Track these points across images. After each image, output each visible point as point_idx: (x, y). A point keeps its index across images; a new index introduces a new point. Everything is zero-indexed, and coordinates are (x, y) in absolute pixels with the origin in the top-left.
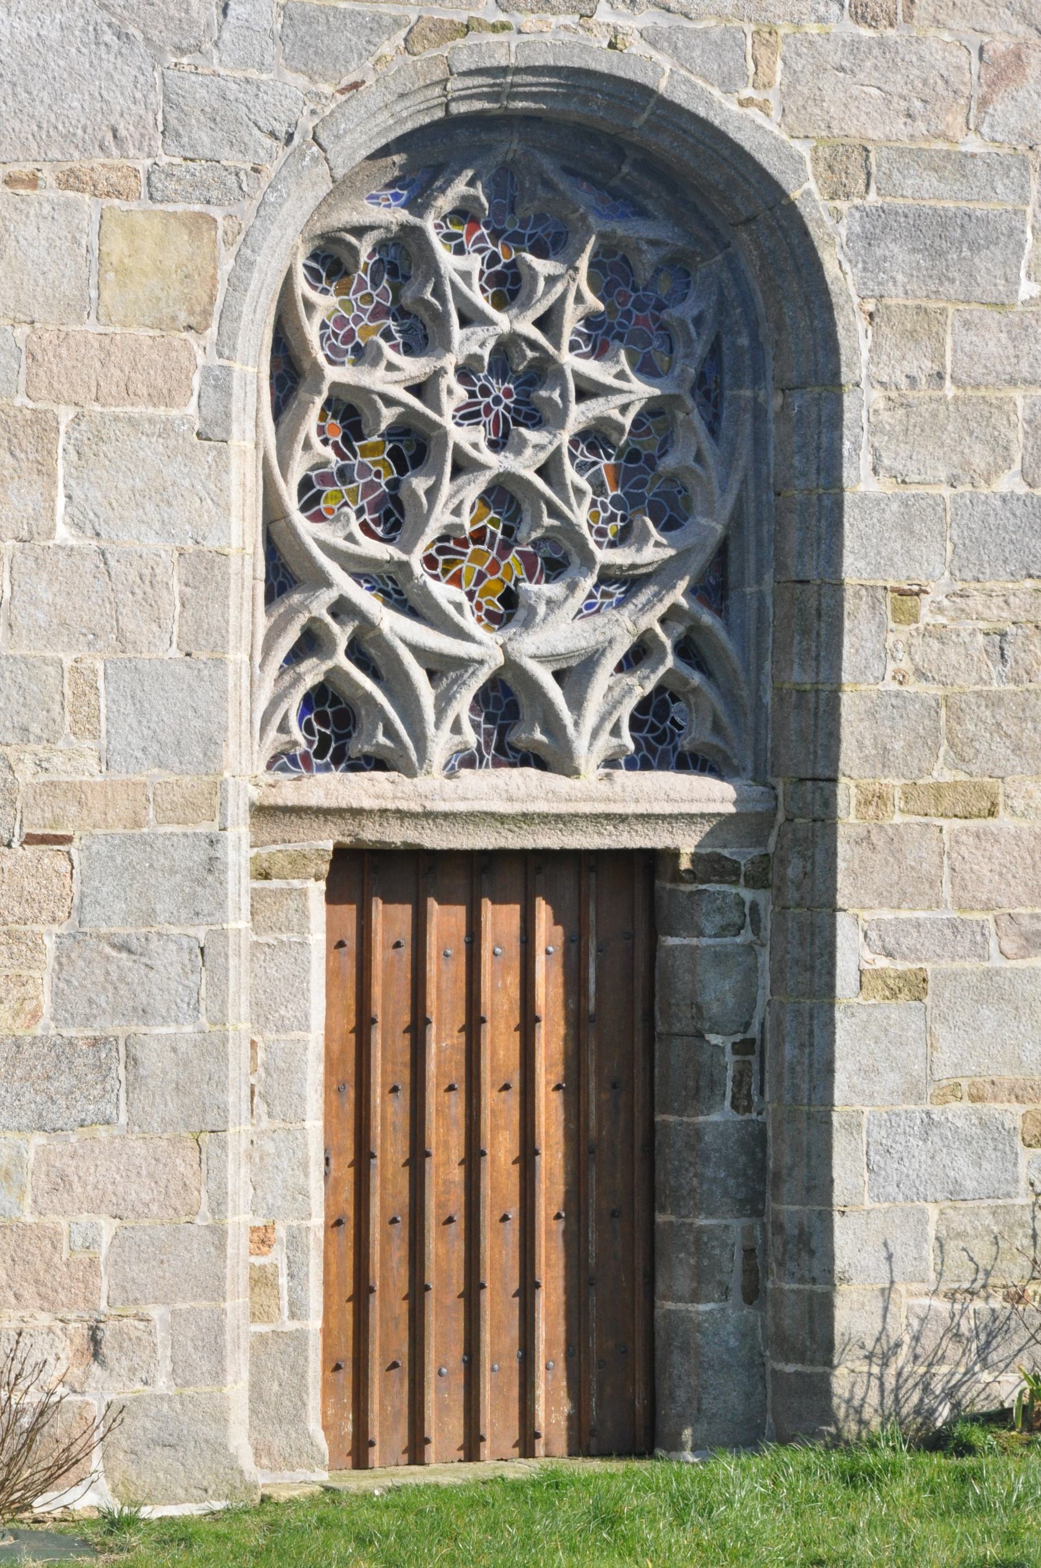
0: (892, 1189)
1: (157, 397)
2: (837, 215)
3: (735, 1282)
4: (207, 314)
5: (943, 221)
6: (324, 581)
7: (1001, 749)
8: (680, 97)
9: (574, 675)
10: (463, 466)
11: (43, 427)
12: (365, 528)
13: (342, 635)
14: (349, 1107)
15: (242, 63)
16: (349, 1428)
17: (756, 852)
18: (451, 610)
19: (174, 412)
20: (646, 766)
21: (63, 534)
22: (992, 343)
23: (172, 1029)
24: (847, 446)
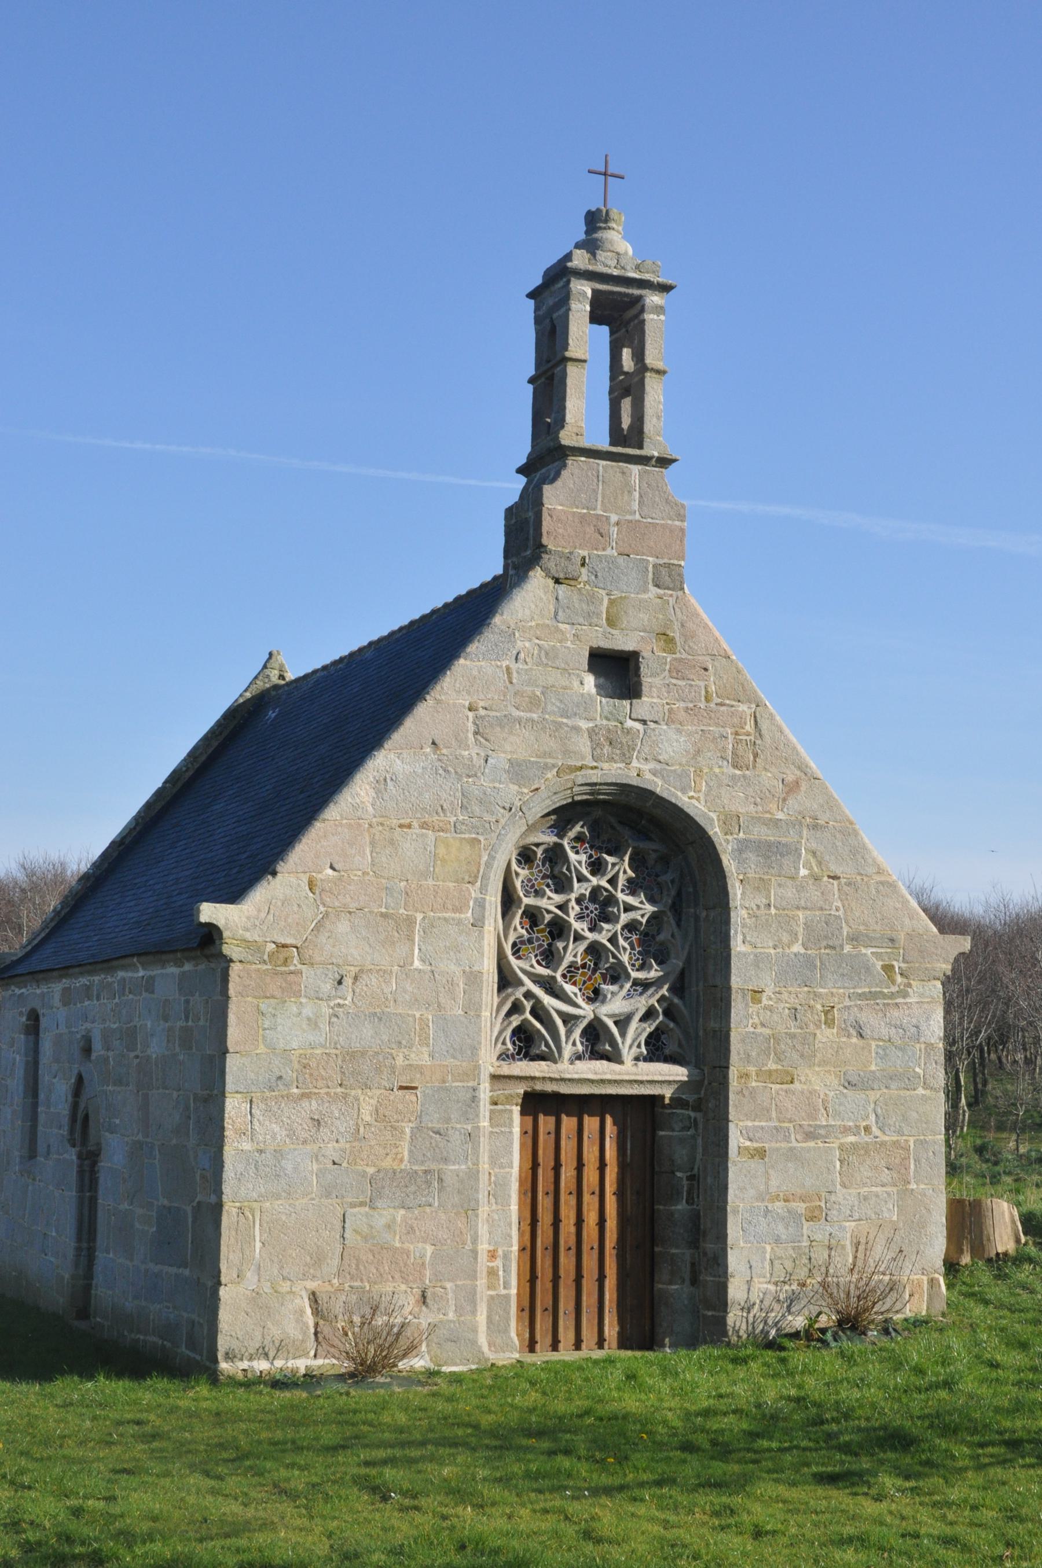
12: (538, 962)
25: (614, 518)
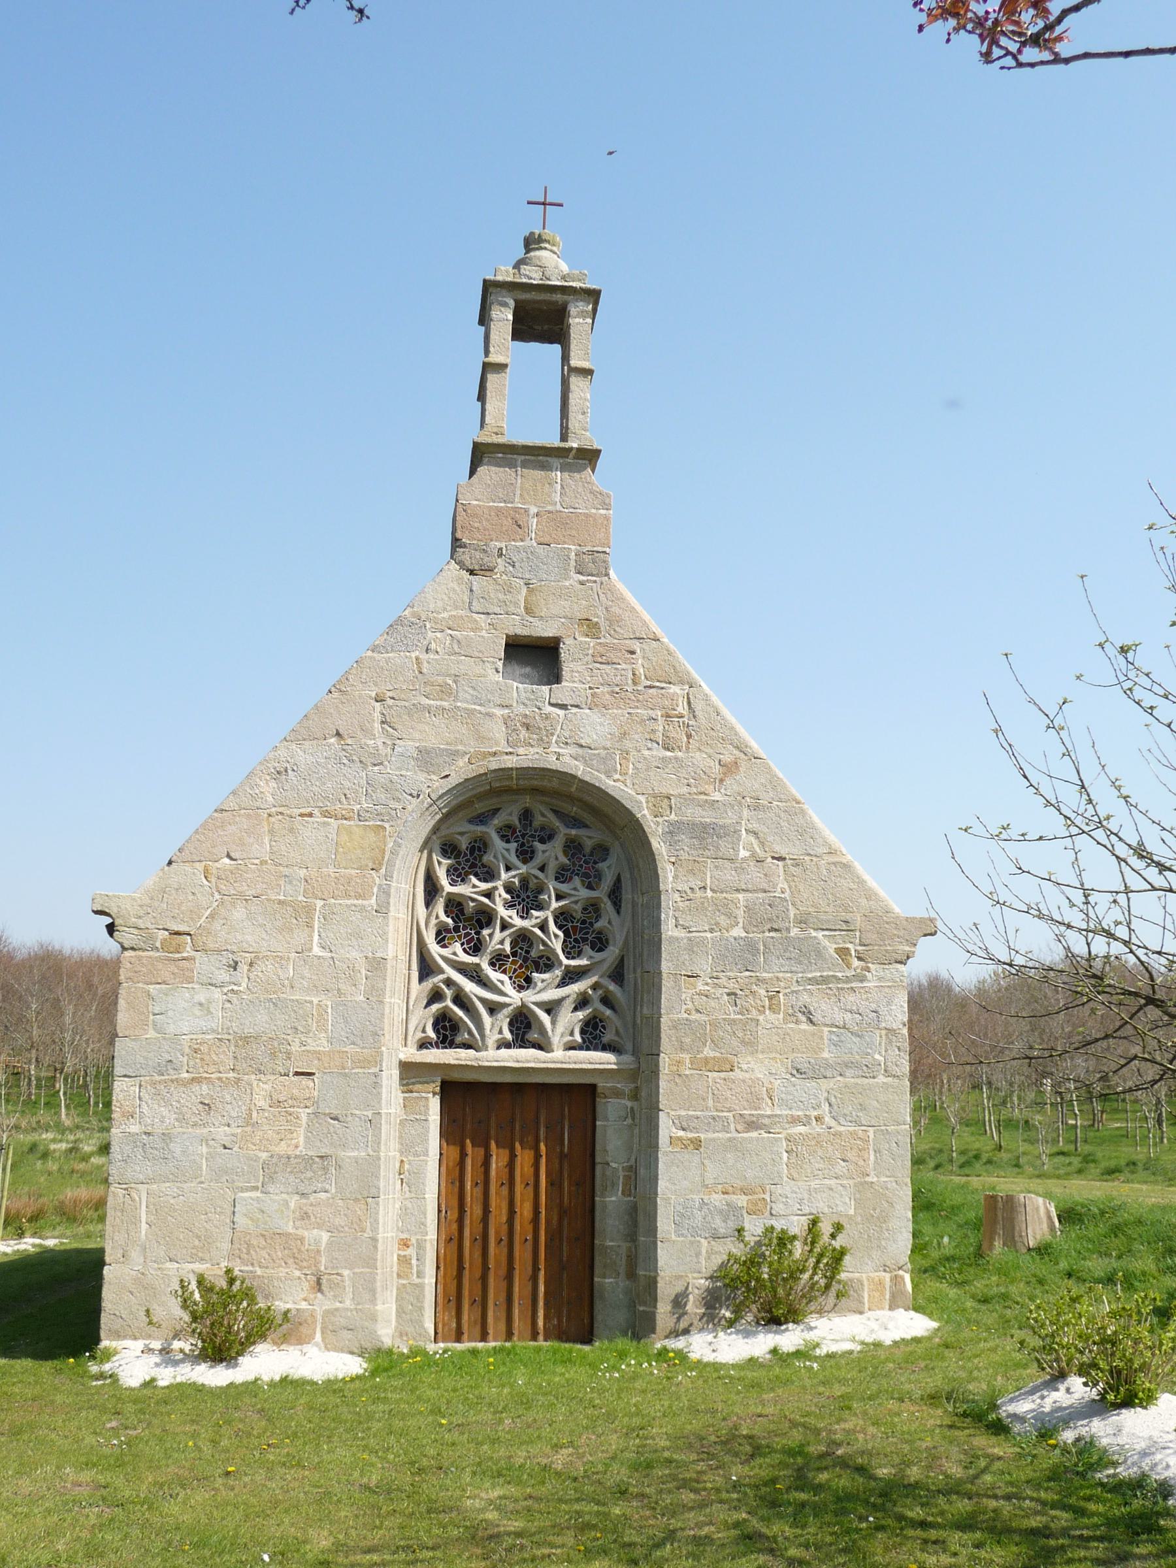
0: (685, 1232)
1: (359, 896)
2: (658, 824)
3: (622, 1270)
4: (381, 864)
5: (705, 826)
6: (442, 971)
7: (735, 1043)
8: (587, 778)
9: (551, 1008)
10: (505, 926)
11: (309, 910)
12: (464, 950)
13: (449, 993)
14: (456, 1190)
15: (400, 769)
16: (454, 1325)
17: (633, 1085)
18: (499, 984)
19: (365, 902)
20: (588, 1049)
21: (317, 950)
22: (729, 875)
23: (356, 1154)
24: (663, 916)
25: (534, 510)
